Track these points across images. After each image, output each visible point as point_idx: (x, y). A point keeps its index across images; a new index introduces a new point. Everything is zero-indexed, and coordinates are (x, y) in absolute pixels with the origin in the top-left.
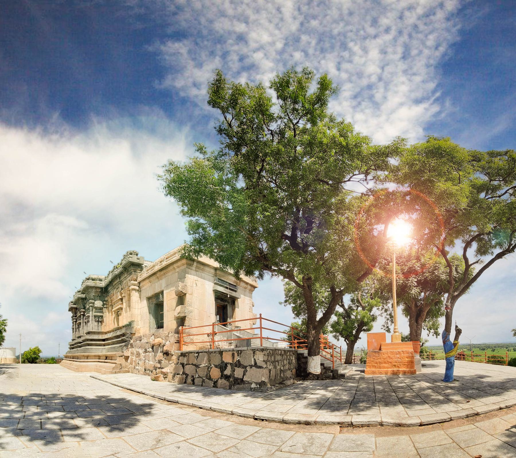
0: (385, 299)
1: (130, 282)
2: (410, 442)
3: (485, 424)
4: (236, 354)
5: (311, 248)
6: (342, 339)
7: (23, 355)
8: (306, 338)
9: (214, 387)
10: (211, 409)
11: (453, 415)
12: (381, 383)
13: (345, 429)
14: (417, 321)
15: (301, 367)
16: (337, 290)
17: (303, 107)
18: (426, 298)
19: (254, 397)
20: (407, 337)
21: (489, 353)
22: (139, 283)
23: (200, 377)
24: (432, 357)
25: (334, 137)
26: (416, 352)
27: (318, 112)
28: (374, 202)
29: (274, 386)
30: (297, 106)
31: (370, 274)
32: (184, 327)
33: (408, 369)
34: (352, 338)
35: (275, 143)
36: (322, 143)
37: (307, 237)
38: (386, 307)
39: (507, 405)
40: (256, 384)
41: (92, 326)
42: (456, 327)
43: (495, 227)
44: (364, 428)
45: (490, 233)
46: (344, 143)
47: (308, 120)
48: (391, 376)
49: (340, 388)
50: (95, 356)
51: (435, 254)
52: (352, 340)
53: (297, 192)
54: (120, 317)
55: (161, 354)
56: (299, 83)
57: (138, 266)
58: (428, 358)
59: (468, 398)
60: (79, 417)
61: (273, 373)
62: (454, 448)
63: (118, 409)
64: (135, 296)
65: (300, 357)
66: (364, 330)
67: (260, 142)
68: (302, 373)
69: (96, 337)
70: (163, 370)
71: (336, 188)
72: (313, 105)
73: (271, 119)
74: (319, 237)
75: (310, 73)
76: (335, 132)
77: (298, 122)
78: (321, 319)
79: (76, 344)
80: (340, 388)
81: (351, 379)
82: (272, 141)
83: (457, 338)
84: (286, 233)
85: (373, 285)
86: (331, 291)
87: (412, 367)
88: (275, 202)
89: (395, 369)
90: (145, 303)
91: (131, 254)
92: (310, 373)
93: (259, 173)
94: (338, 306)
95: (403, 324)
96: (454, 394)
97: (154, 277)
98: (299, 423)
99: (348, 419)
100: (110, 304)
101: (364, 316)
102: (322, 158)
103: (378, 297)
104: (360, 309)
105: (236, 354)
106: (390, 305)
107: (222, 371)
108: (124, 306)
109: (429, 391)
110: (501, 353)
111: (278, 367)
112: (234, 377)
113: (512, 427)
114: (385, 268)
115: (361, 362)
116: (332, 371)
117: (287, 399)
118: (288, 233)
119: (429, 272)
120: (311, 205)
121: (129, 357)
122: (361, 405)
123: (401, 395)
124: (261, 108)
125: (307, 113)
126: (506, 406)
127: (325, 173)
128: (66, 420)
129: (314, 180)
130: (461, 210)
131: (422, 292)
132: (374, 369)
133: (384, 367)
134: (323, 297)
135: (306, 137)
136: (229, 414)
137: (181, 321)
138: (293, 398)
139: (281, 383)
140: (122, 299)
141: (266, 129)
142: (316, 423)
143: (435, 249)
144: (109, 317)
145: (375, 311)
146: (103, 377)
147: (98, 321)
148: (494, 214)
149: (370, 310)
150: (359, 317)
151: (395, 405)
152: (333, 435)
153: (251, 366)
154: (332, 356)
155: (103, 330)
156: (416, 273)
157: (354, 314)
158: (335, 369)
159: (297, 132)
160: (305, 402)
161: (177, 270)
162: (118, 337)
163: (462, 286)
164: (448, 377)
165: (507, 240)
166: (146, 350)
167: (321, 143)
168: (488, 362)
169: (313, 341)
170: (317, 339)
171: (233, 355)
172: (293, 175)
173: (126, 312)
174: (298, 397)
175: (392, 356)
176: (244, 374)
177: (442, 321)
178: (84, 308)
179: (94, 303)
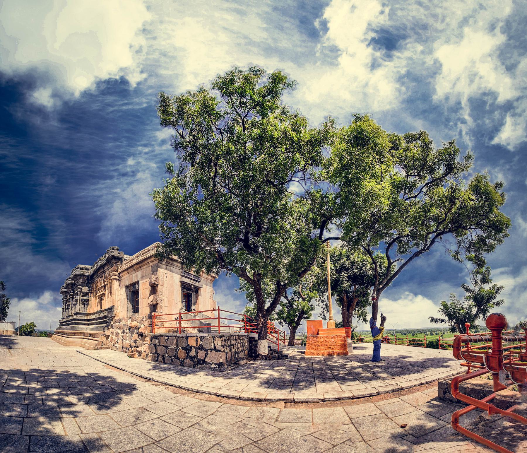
0: (322, 292)
1: (111, 272)
2: (344, 413)
3: (409, 397)
4: (199, 340)
5: (260, 249)
8: (257, 322)
9: (180, 365)
10: (180, 387)
11: (382, 390)
12: (318, 362)
13: (289, 405)
14: (348, 310)
15: (252, 349)
16: (282, 283)
18: (356, 291)
19: (214, 376)
20: (340, 324)
21: (410, 337)
22: (119, 274)
23: (170, 357)
24: (362, 340)
27: (268, 103)
28: (311, 207)
29: (231, 365)
30: (244, 100)
31: (309, 270)
32: (156, 314)
33: (341, 351)
34: (294, 324)
35: (225, 143)
36: (272, 137)
37: (257, 240)
38: (322, 299)
39: (427, 381)
40: (216, 364)
41: (79, 308)
42: (382, 315)
44: (304, 404)
45: (408, 235)
46: (296, 139)
48: (327, 357)
49: (284, 368)
50: (81, 333)
51: (362, 253)
52: (294, 326)
53: (248, 196)
55: (137, 335)
58: (358, 341)
59: (394, 375)
60: (72, 394)
61: (229, 355)
62: (383, 418)
63: (103, 387)
65: (251, 340)
66: (304, 318)
67: (211, 144)
68: (253, 354)
69: (82, 317)
70: (137, 349)
71: (280, 193)
72: (264, 97)
73: (219, 117)
76: (287, 125)
78: (269, 308)
79: (65, 322)
80: (284, 368)
81: (293, 359)
82: (222, 140)
83: (382, 324)
85: (312, 280)
86: (277, 284)
87: (345, 349)
88: (229, 210)
89: (331, 351)
90: (123, 290)
92: (259, 355)
93: (214, 179)
94: (282, 297)
95: (336, 314)
96: (381, 372)
97: (132, 269)
98: (252, 400)
99: (291, 397)
100: (95, 289)
101: (304, 306)
102: (272, 155)
103: (316, 290)
104: (301, 300)
105: (199, 340)
106: (326, 297)
107: (188, 353)
108: (107, 292)
109: (359, 370)
110: (420, 337)
111: (233, 350)
112: (197, 358)
113: (432, 400)
114: (321, 266)
115: (302, 345)
116: (277, 353)
117: (241, 378)
118: (242, 236)
119: (358, 269)
120: (260, 210)
121: (109, 336)
122: (301, 384)
123: (335, 373)
124: (207, 109)
126: (426, 382)
127: (275, 173)
128: (62, 397)
129: (264, 181)
130: (384, 214)
131: (352, 285)
132: (312, 351)
134: (270, 289)
135: (255, 130)
136: (194, 392)
137: (154, 307)
138: (247, 378)
139: (235, 363)
140: (104, 287)
142: (265, 400)
143: (362, 249)
144: (94, 301)
145: (313, 302)
146: (87, 352)
147: (84, 304)
148: (411, 217)
149: (309, 301)
150: (300, 307)
151: (331, 381)
152: (279, 410)
153: (212, 350)
154: (277, 339)
156: (347, 270)
157: (296, 304)
158: (280, 351)
159: (247, 126)
160: (257, 382)
161: (151, 264)
163: (386, 280)
164: (376, 357)
165: (423, 241)
166: (124, 330)
167: (271, 136)
168: (410, 345)
169: (262, 327)
171: (197, 340)
172: (244, 176)
174: (250, 377)
175: (327, 340)
176: (206, 356)
177: (369, 310)
178: (74, 292)
179: (81, 289)
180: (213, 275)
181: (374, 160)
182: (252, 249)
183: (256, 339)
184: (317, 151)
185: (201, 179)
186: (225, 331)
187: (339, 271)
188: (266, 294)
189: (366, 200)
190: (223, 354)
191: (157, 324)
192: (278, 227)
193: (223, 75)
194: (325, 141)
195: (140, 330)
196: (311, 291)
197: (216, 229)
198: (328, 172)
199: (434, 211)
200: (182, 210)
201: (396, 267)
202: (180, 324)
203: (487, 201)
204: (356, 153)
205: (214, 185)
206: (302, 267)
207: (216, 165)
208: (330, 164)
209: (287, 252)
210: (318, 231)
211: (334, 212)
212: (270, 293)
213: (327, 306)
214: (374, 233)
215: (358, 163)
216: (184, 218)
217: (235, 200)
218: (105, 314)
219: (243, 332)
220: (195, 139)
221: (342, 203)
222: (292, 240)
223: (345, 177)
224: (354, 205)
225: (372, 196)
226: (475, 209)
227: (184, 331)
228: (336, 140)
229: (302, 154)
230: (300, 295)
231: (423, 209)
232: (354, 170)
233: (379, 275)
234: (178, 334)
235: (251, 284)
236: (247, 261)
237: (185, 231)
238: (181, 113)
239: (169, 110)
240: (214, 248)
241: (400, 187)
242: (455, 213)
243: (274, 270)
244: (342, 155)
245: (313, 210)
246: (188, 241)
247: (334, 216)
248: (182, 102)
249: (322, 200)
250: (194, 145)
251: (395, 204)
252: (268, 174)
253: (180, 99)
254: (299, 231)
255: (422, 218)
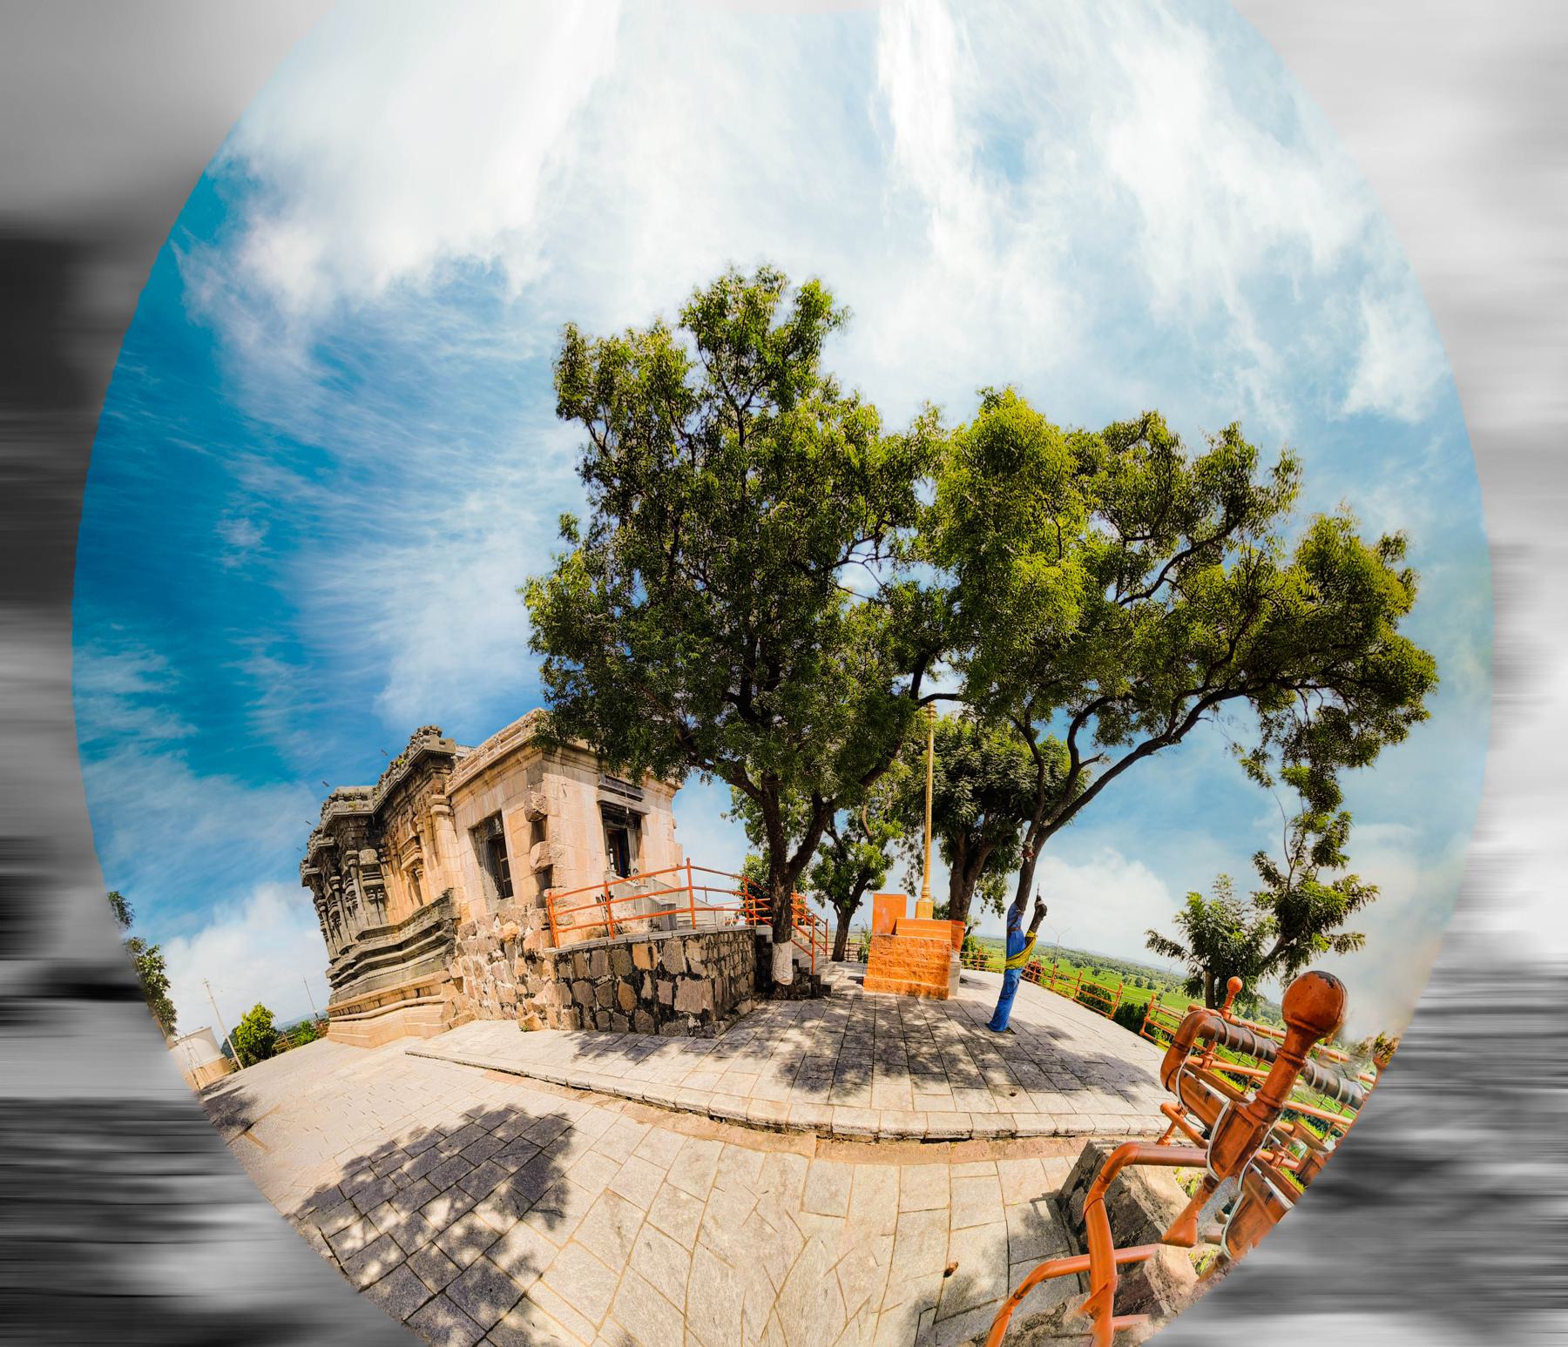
0: (911, 824)
5: (777, 718)
6: (830, 904)
7: (234, 1036)
12: (886, 1012)
14: (965, 878)
16: (825, 799)
17: (759, 360)
18: (987, 828)
22: (450, 797)
25: (831, 445)
26: (955, 946)
27: (795, 371)
30: (745, 362)
31: (886, 770)
35: (698, 470)
36: (804, 459)
38: (911, 841)
43: (1139, 683)
45: (1127, 696)
46: (855, 462)
47: (772, 396)
48: (906, 998)
52: (846, 911)
53: (748, 596)
54: (421, 883)
56: (750, 303)
57: (443, 760)
64: (444, 826)
66: (869, 887)
67: (668, 472)
69: (381, 942)
71: (823, 589)
72: (786, 353)
73: (688, 406)
74: (793, 697)
75: (776, 279)
76: (833, 428)
77: (748, 404)
78: (795, 858)
79: (343, 970)
82: (692, 464)
84: (732, 690)
87: (943, 982)
88: (705, 628)
89: (915, 982)
90: (466, 842)
91: (426, 733)
93: (670, 558)
94: (824, 834)
95: (938, 881)
97: (479, 782)
104: (864, 840)
106: (919, 837)
108: (426, 853)
111: (726, 973)
114: (914, 760)
118: (734, 690)
124: (664, 383)
125: (769, 377)
127: (809, 544)
129: (785, 564)
130: (1066, 640)
132: (878, 978)
133: (897, 975)
135: (767, 441)
140: (417, 839)
141: (677, 436)
143: (1011, 725)
144: (396, 885)
145: (892, 848)
149: (882, 845)
155: (393, 919)
156: (972, 773)
159: (748, 431)
162: (426, 933)
164: (998, 1021)
167: (802, 457)
169: (780, 909)
170: (787, 901)
173: (432, 868)
175: (912, 950)
180: (671, 781)
181: (1038, 506)
182: (756, 719)
183: (770, 939)
184: (905, 490)
185: (640, 557)
186: (706, 921)
187: (953, 775)
188: (789, 823)
189: (1023, 606)
190: (707, 985)
191: (560, 919)
192: (817, 668)
193: (705, 290)
194: (921, 465)
195: (526, 946)
196: (887, 821)
197: (675, 672)
198: (931, 540)
199: (1199, 632)
200: (595, 629)
201: (1092, 774)
202: (609, 911)
203: (1357, 601)
204: (995, 490)
205: (672, 572)
206: (871, 762)
207: (677, 523)
208: (936, 521)
209: (838, 725)
210: (908, 679)
211: (946, 634)
212: (799, 823)
213: (920, 862)
214: (1042, 686)
215: (1002, 515)
216: (601, 649)
217: (719, 606)
218: (435, 917)
219: (742, 922)
220: (633, 457)
221: (965, 611)
222: (848, 699)
223: (971, 550)
224: (994, 617)
225: (1036, 596)
226: (1318, 624)
227: (620, 931)
228: (947, 461)
229: (871, 499)
230: (863, 828)
231: (1168, 626)
232: (991, 534)
233: (1047, 792)
234: (611, 941)
235: (757, 800)
236: (747, 747)
237: (602, 678)
238: (606, 385)
239: (580, 374)
240: (672, 718)
241: (1109, 568)
242: (1260, 637)
243: (808, 768)
244: (963, 498)
245: (897, 629)
246: (609, 703)
247: (946, 645)
248: (613, 358)
249: (918, 607)
250: (627, 473)
251: (1095, 614)
252: (795, 546)
253: (608, 348)
254: (864, 678)
255: (1166, 651)
